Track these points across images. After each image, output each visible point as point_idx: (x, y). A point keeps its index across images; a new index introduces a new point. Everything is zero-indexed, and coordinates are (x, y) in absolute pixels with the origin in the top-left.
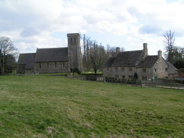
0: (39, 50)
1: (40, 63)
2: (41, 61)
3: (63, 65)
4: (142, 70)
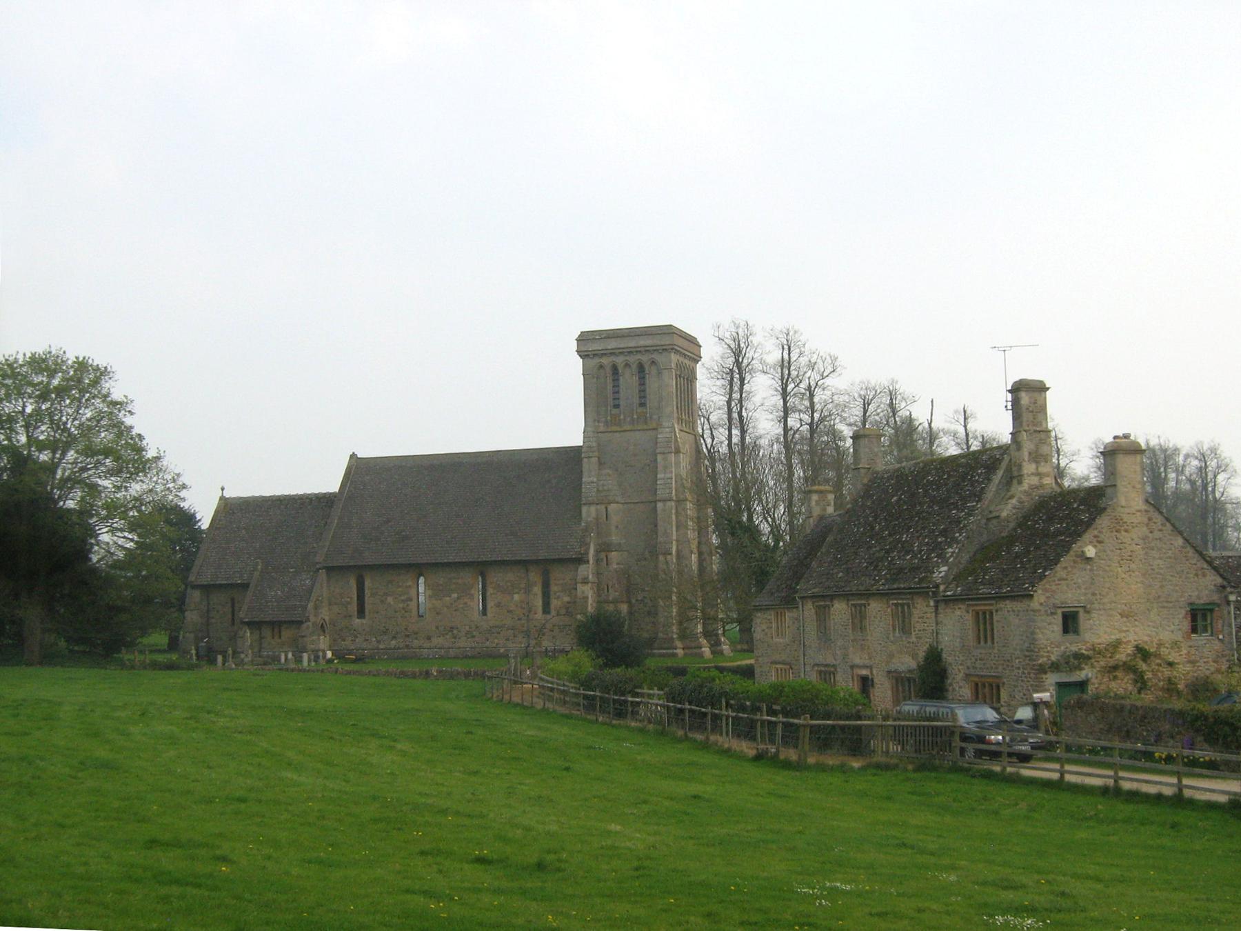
0: (359, 470)
1: (360, 572)
2: (369, 558)
3: (537, 590)
4: (969, 618)
